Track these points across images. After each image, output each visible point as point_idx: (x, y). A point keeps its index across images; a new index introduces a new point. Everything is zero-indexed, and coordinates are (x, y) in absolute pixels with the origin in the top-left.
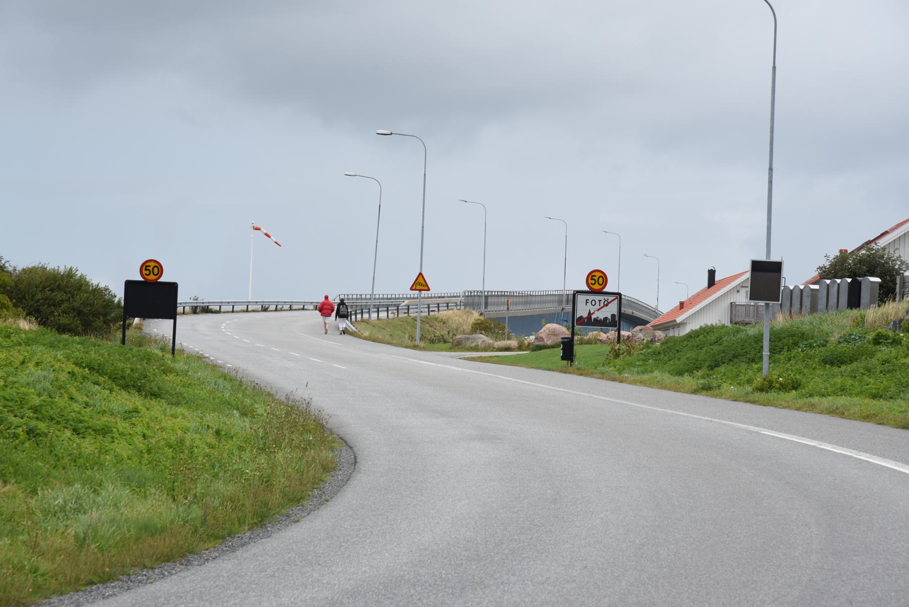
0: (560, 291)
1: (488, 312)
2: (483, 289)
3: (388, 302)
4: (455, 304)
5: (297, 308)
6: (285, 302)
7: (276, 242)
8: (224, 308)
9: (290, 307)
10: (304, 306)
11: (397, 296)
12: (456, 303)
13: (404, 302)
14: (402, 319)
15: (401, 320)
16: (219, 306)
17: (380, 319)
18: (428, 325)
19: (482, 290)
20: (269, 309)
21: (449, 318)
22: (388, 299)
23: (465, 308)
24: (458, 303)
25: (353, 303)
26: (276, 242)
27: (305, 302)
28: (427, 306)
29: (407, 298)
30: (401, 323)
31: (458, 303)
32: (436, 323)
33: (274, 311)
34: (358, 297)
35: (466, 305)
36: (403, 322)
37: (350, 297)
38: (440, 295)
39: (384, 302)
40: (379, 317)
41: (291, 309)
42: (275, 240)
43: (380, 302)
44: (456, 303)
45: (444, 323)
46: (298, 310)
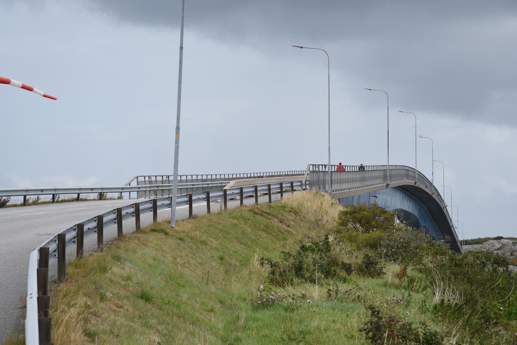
0: (322, 165)
1: (348, 190)
2: (388, 164)
3: (203, 184)
4: (300, 184)
5: (66, 198)
6: (42, 190)
7: (45, 96)
8: (43, 198)
9: (53, 198)
10: (79, 194)
11: (214, 177)
12: (301, 182)
13: (229, 183)
14: (235, 213)
15: (231, 214)
16: (23, 197)
17: (195, 217)
18: (276, 220)
19: (387, 165)
20: (8, 204)
21: (300, 205)
22: (203, 180)
23: (311, 189)
24: (304, 182)
25: (157, 187)
26: (45, 96)
27: (80, 189)
28: (238, 191)
29: (232, 179)
30: (235, 221)
31: (304, 182)
32: (286, 215)
33: (21, 205)
34: (164, 178)
35: (312, 184)
36: (238, 220)
37: (153, 179)
38: (259, 175)
39: (198, 185)
40: (194, 212)
41: (25, 203)
42: (43, 93)
43: (193, 185)
44: (301, 182)
45: (296, 213)
46: (69, 201)
